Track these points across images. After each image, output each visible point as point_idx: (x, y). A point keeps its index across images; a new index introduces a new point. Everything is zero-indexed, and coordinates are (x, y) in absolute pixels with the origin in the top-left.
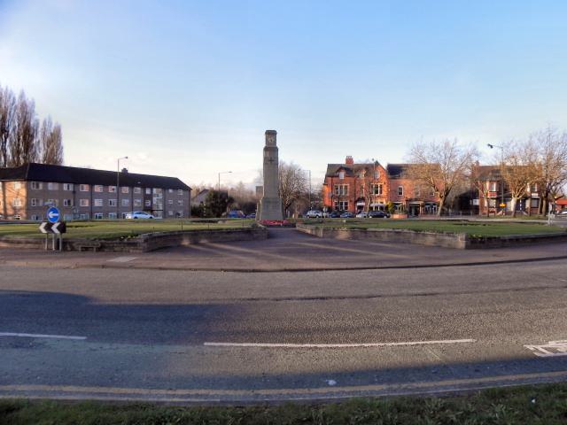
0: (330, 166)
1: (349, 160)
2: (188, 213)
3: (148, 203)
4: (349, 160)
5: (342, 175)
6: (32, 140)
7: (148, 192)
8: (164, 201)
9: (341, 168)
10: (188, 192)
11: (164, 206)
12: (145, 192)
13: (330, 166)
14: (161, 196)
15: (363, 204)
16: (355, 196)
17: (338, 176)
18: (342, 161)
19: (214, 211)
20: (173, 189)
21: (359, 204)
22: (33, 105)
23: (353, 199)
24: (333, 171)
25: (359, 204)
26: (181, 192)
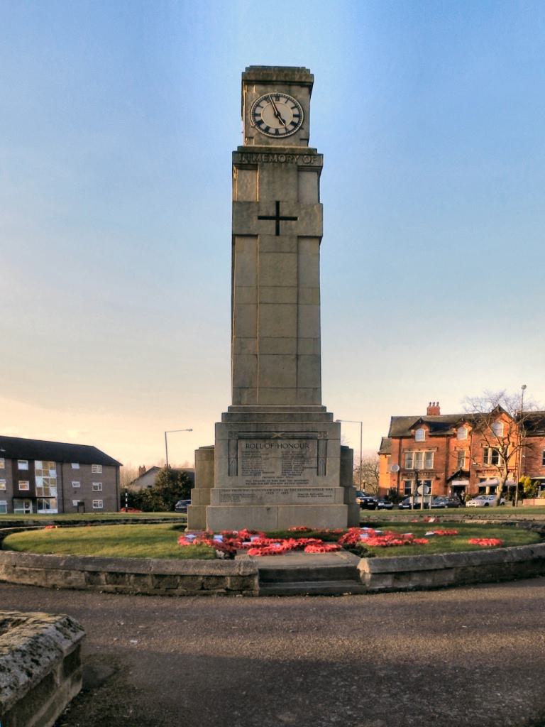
0: (395, 420)
1: (434, 409)
2: (114, 503)
3: (24, 486)
4: (434, 409)
5: (421, 434)
6: (359, 574)
7: (23, 466)
8: (61, 482)
9: (419, 423)
10: (113, 470)
11: (62, 491)
12: (15, 467)
13: (395, 420)
14: (53, 474)
15: (465, 482)
16: (446, 471)
17: (413, 437)
18: (422, 412)
19: (166, 500)
20: (81, 463)
21: (455, 483)
22: (344, 437)
23: (442, 475)
24: (402, 430)
25: (455, 483)
26: (98, 469)
